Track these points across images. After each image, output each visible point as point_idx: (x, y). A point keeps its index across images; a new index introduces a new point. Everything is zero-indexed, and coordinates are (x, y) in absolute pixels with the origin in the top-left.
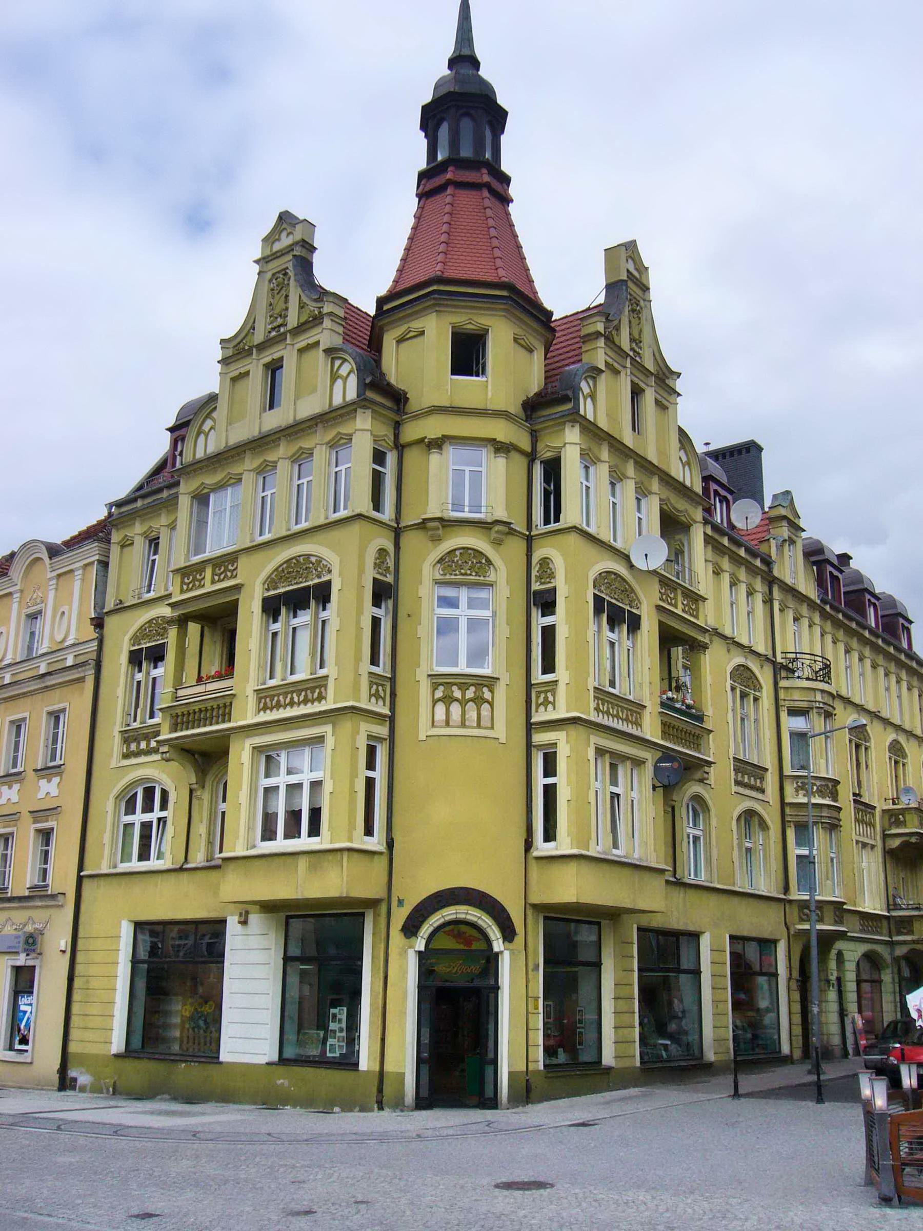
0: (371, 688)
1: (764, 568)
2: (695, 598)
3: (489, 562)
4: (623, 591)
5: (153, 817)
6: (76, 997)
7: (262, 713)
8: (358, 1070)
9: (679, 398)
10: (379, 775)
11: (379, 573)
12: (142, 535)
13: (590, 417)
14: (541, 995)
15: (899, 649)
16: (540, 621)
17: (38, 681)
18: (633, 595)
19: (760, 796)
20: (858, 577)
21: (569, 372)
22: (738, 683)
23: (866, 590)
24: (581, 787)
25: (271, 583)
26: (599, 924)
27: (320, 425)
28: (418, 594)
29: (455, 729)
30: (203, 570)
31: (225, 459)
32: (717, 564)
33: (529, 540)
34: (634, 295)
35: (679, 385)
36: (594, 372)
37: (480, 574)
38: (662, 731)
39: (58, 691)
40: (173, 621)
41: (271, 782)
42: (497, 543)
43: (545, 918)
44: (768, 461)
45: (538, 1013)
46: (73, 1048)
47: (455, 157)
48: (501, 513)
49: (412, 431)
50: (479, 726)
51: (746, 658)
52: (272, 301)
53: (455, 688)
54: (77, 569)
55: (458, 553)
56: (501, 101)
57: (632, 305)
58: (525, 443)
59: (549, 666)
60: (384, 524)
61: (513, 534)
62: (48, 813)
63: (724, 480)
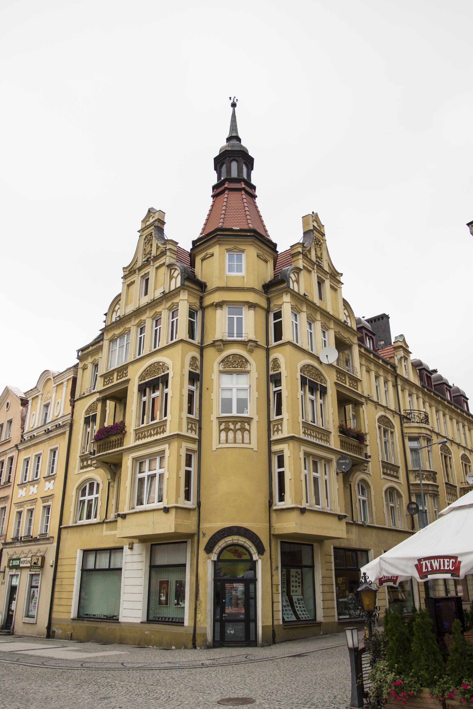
0: (188, 425)
1: (392, 369)
2: (355, 381)
3: (247, 361)
4: (317, 375)
5: (92, 497)
6: (57, 589)
7: (137, 441)
8: (183, 626)
9: (343, 285)
10: (193, 469)
11: (192, 368)
12: (91, 363)
13: (296, 290)
14: (280, 583)
15: (463, 411)
16: (273, 389)
17: (46, 435)
18: (322, 377)
19: (396, 480)
20: (440, 378)
21: (284, 270)
22: (382, 424)
23: (444, 383)
24: (297, 473)
25: (142, 377)
26: (312, 545)
27: (164, 300)
28: (211, 378)
29: (231, 444)
30: (112, 375)
31: (123, 321)
32: (368, 367)
33: (268, 350)
34: (317, 237)
35: (342, 279)
36: (298, 270)
37: (242, 367)
38: (341, 445)
39: (55, 439)
40: (99, 400)
41: (141, 475)
42: (251, 351)
43: (281, 542)
44: (392, 323)
45: (279, 593)
46: (54, 615)
47: (228, 177)
48: (252, 337)
49: (209, 300)
50: (243, 442)
51: (385, 412)
52: (145, 248)
53: (230, 424)
54: (65, 381)
55: (231, 357)
56: (250, 154)
57: (316, 241)
58: (264, 304)
59: (279, 412)
60: (196, 345)
61: (258, 347)
62: (48, 498)
63: (370, 329)
